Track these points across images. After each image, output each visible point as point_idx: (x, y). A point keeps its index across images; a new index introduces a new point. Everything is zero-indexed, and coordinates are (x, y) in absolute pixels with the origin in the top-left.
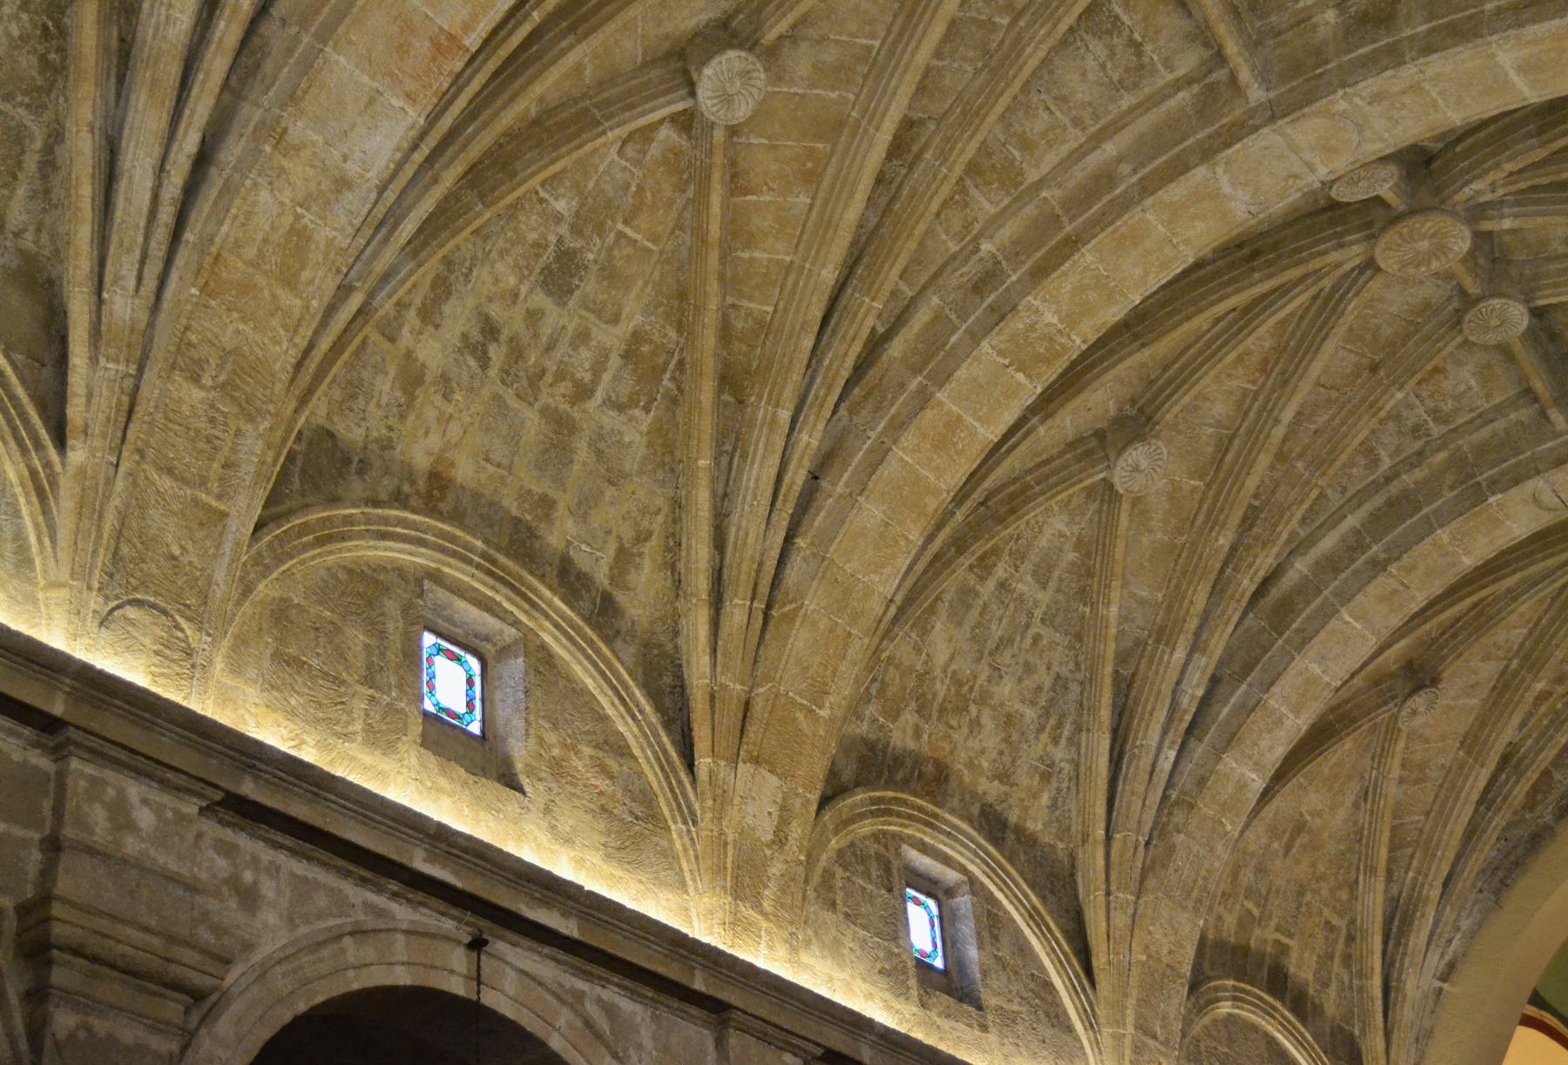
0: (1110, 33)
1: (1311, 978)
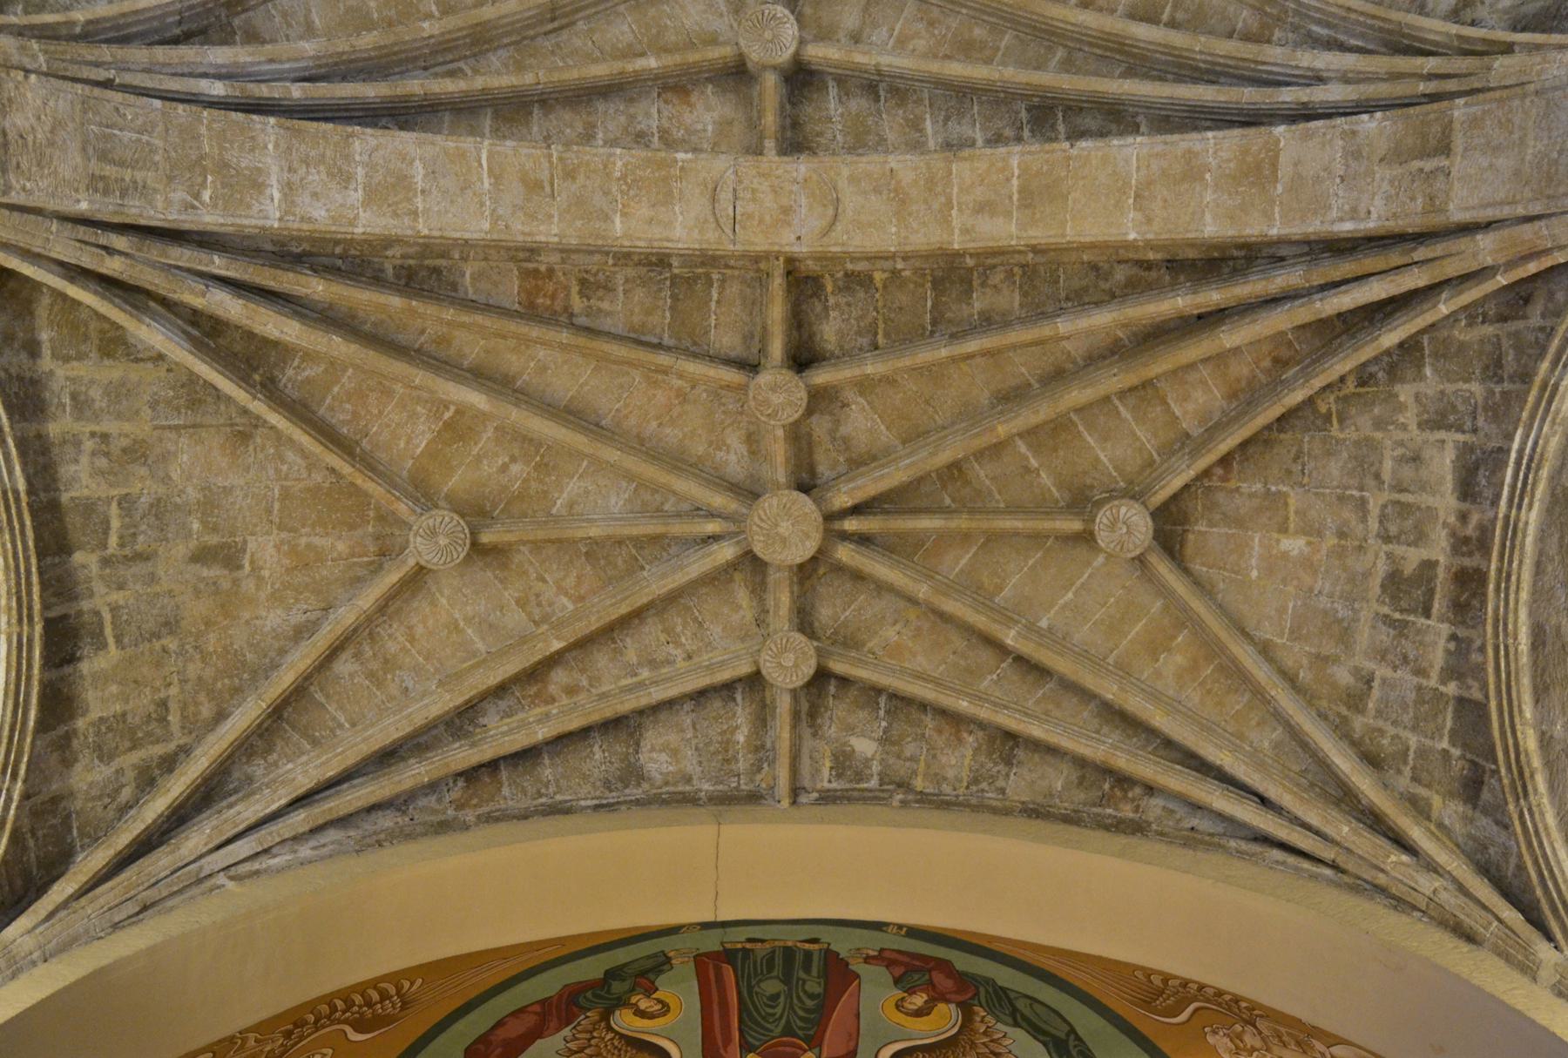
1: (94, 714)
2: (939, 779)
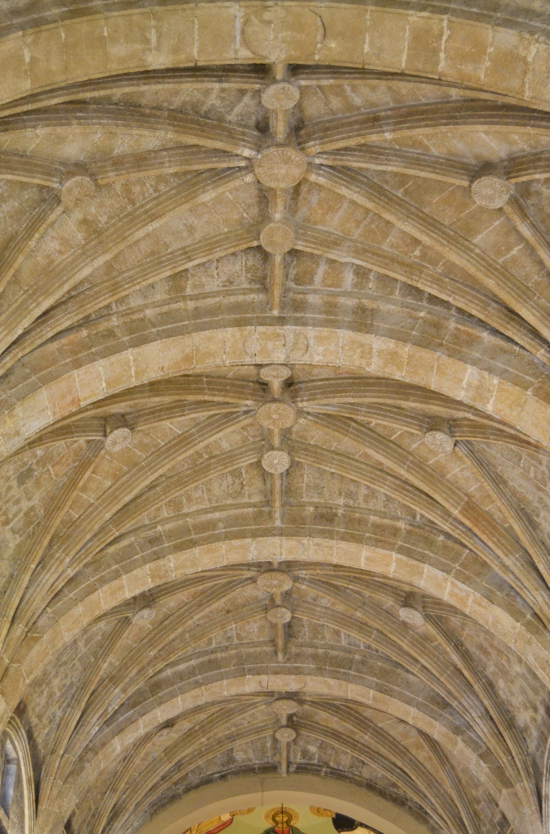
0: (236, 477)
2: (339, 764)
